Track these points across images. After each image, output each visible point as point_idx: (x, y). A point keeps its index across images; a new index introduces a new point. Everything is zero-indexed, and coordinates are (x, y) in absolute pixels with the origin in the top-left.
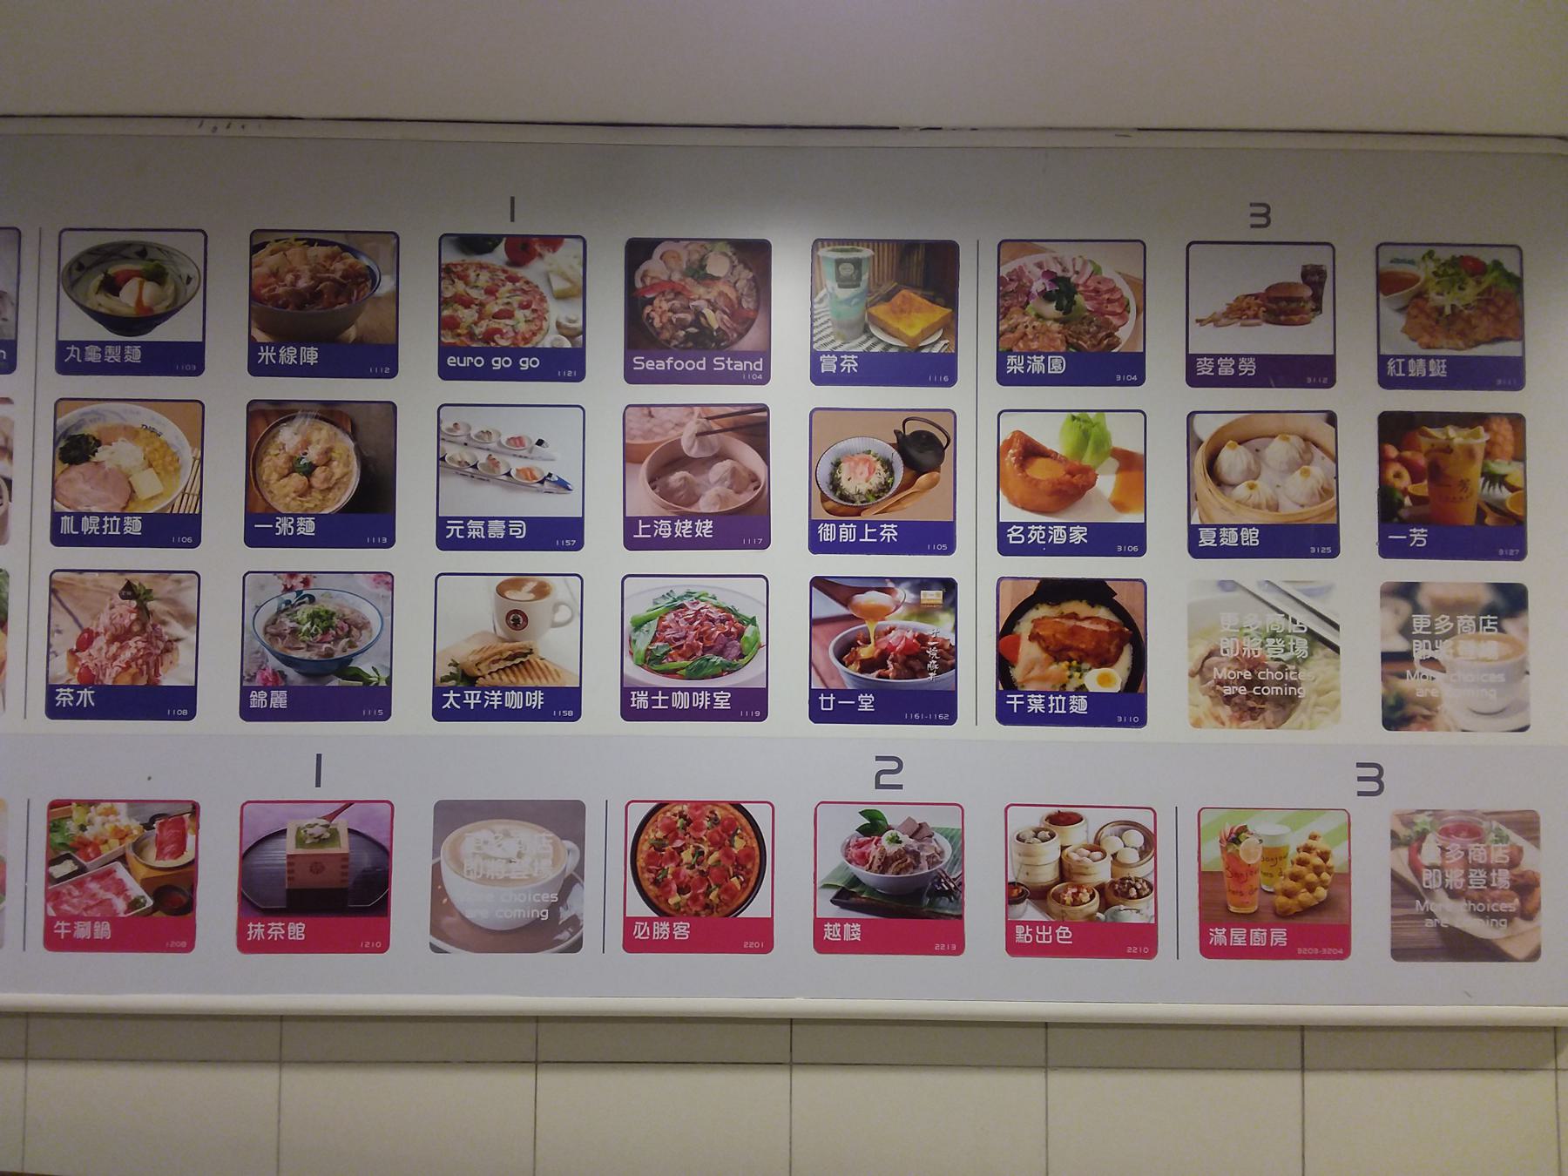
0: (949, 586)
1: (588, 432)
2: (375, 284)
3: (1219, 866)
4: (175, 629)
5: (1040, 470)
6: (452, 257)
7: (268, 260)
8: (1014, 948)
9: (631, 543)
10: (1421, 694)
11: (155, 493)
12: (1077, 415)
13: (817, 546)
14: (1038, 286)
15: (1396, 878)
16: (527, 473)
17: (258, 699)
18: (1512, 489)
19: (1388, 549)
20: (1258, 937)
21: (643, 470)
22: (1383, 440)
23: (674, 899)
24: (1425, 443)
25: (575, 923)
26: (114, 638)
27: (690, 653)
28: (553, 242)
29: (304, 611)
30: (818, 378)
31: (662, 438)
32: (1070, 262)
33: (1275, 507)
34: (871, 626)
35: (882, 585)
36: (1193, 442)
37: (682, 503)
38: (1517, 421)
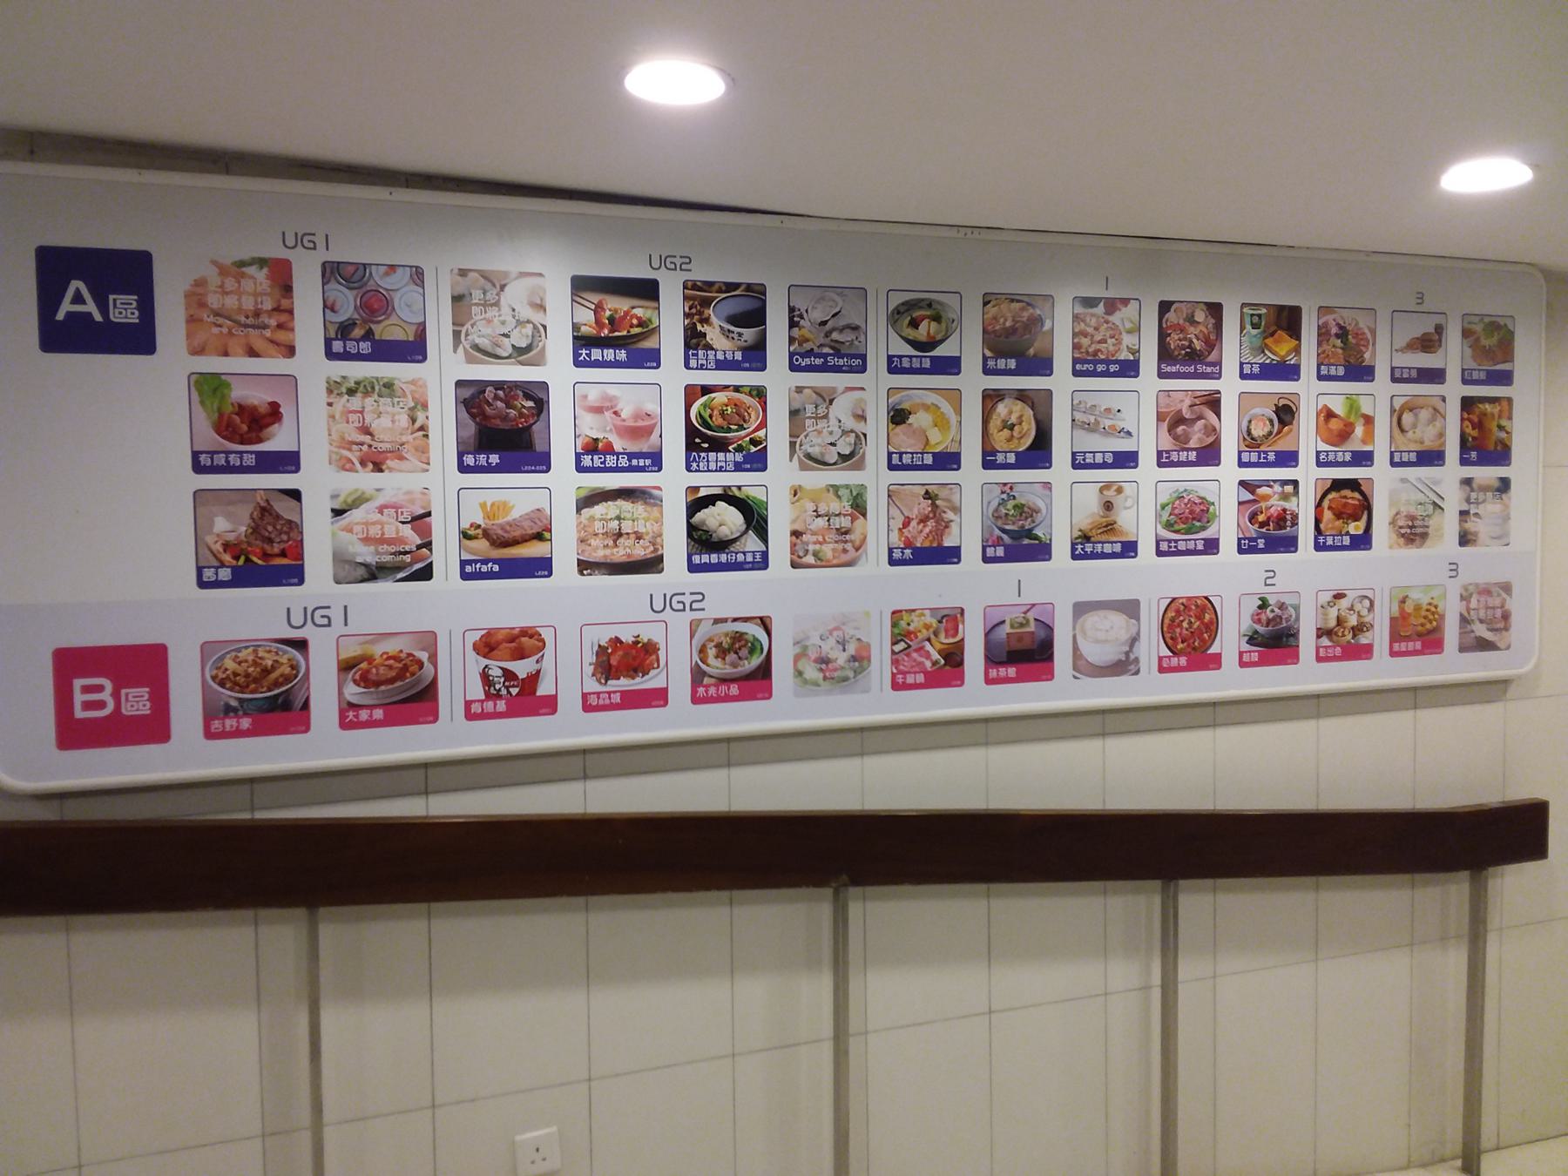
0: (1295, 483)
4: (950, 515)
5: (1335, 424)
6: (1079, 309)
7: (992, 310)
11: (939, 442)
12: (1349, 396)
13: (1241, 464)
16: (1113, 427)
17: (990, 552)
21: (1165, 425)
23: (1180, 646)
25: (1137, 660)
26: (922, 521)
28: (1125, 302)
29: (1010, 504)
32: (1347, 318)
35: (1267, 483)
36: (1393, 411)
37: (1182, 442)
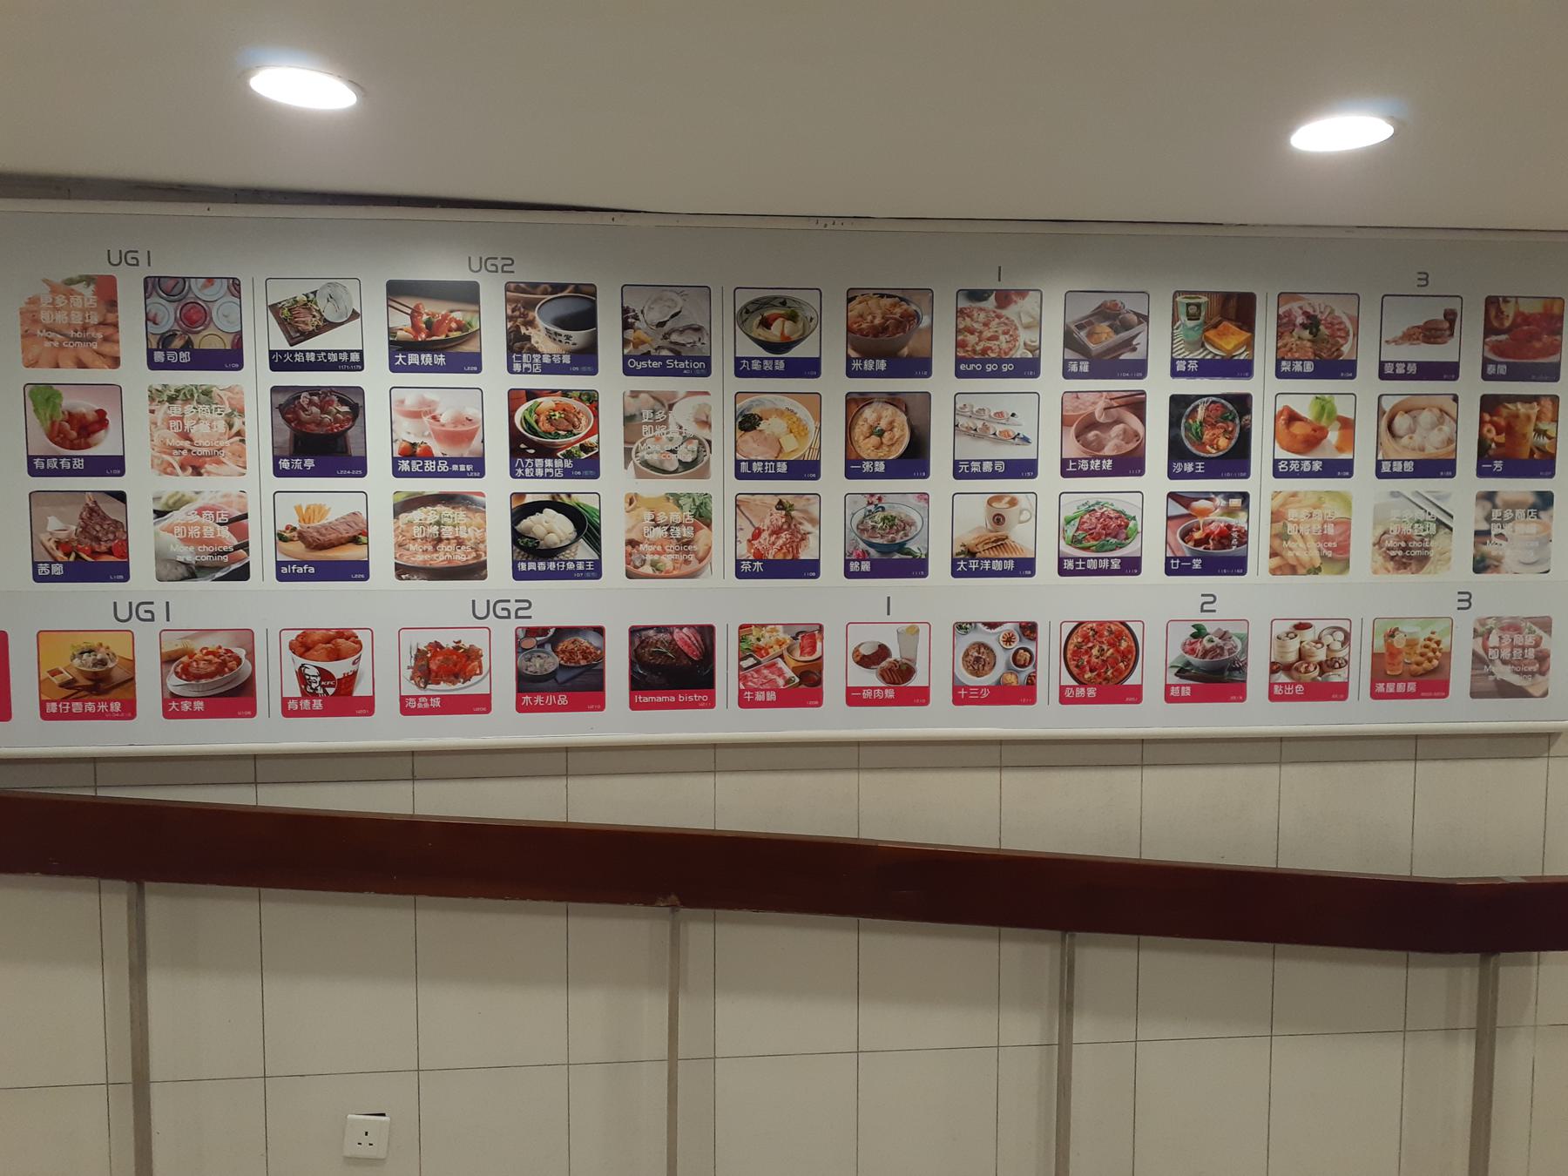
0: (1244, 496)
1: (1041, 408)
2: (919, 322)
3: (1383, 650)
4: (807, 527)
5: (1298, 429)
6: (964, 303)
7: (857, 307)
8: (1273, 697)
9: (1065, 474)
10: (1494, 553)
11: (794, 449)
12: (1318, 396)
14: (1300, 320)
15: (1475, 654)
17: (854, 566)
18: (1550, 438)
19: (1482, 473)
20: (1401, 687)
22: (1482, 410)
24: (1504, 412)
26: (773, 533)
27: (1097, 537)
30: (1175, 373)
31: (1084, 412)
32: (1318, 306)
33: (1422, 449)
34: (1201, 521)
35: (1207, 496)
37: (1094, 450)
38: (1555, 399)
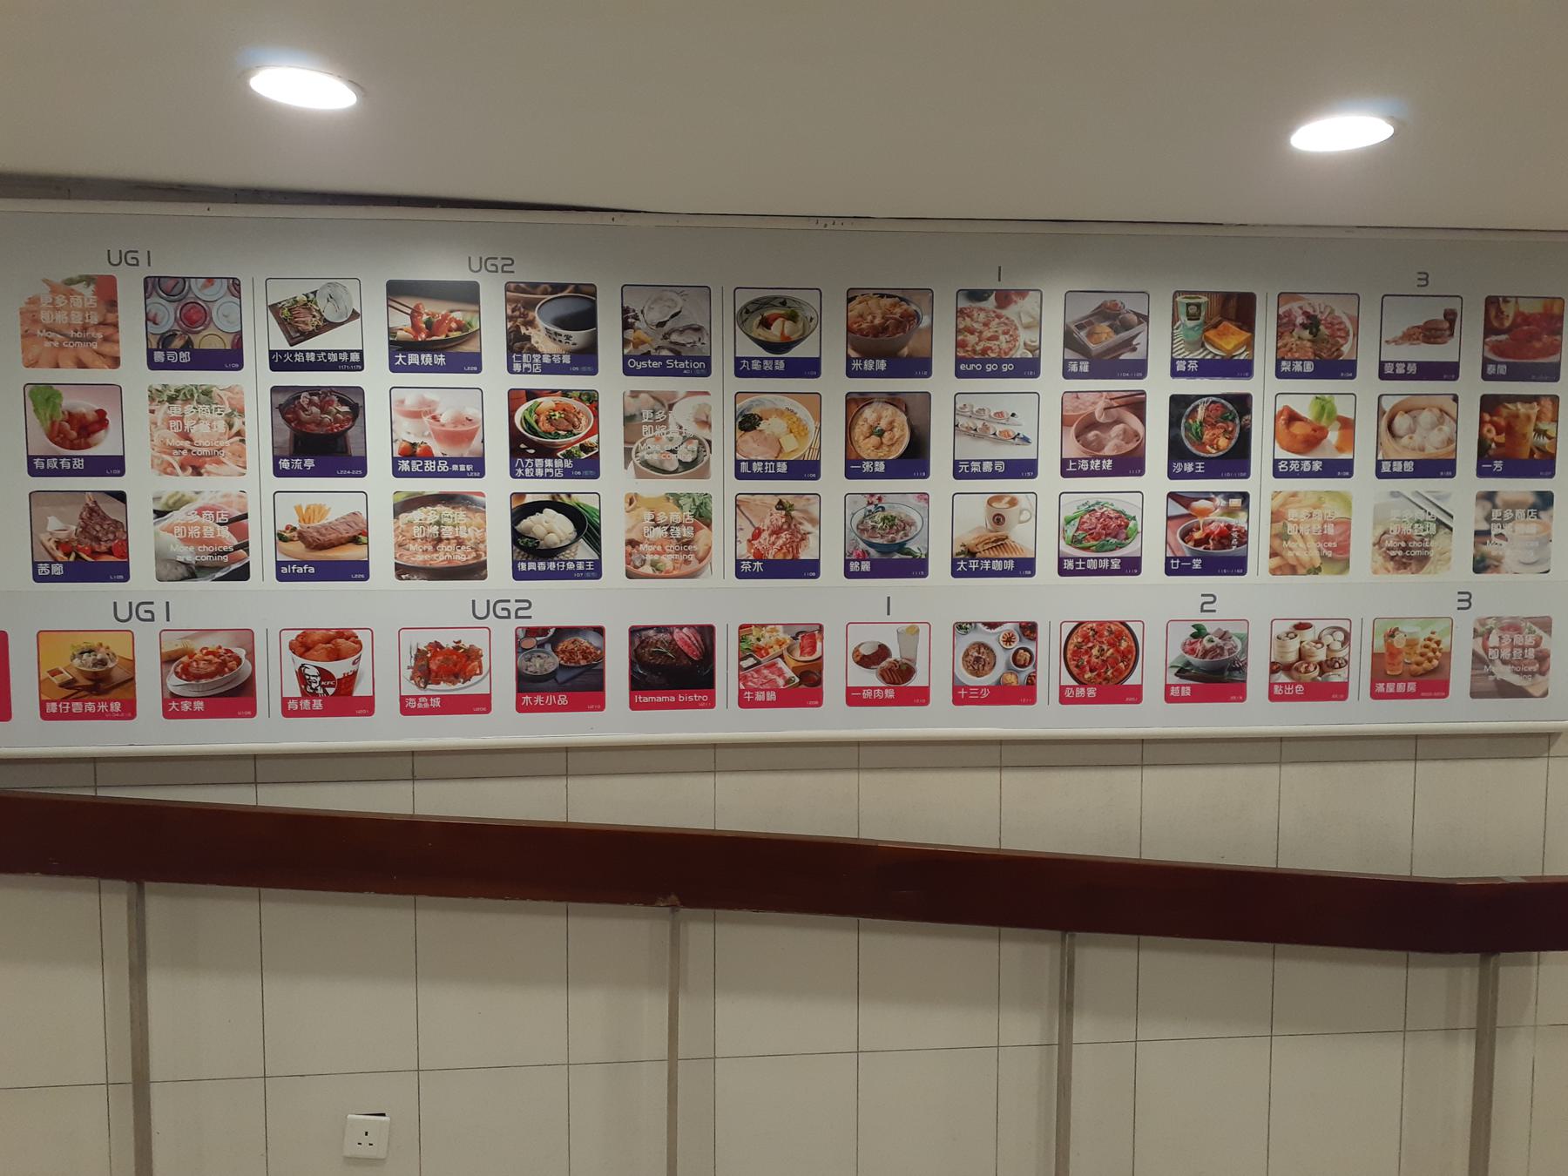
0: (1244, 496)
1: (1041, 408)
2: (919, 322)
3: (1383, 650)
4: (807, 527)
5: (1298, 429)
6: (964, 303)
7: (857, 307)
8: (1273, 697)
9: (1065, 474)
10: (1494, 553)
11: (794, 449)
12: (1318, 396)
14: (1300, 320)
15: (1475, 654)
17: (854, 566)
18: (1550, 438)
19: (1482, 473)
20: (1401, 687)
22: (1482, 410)
24: (1504, 412)
26: (773, 533)
27: (1097, 537)
30: (1175, 373)
31: (1084, 412)
32: (1318, 306)
33: (1422, 449)
34: (1201, 521)
35: (1207, 496)
37: (1094, 450)
38: (1555, 399)
